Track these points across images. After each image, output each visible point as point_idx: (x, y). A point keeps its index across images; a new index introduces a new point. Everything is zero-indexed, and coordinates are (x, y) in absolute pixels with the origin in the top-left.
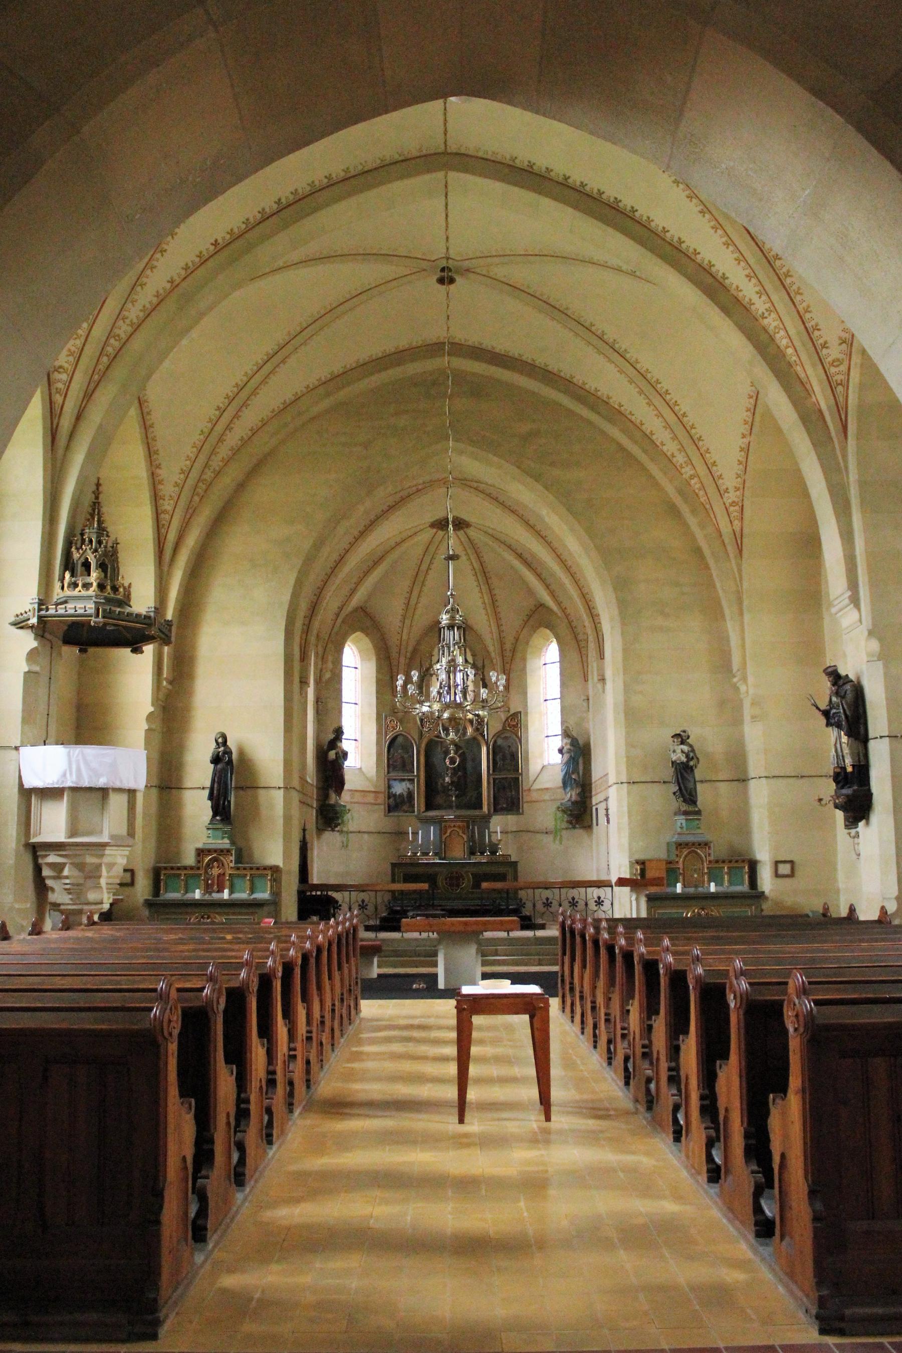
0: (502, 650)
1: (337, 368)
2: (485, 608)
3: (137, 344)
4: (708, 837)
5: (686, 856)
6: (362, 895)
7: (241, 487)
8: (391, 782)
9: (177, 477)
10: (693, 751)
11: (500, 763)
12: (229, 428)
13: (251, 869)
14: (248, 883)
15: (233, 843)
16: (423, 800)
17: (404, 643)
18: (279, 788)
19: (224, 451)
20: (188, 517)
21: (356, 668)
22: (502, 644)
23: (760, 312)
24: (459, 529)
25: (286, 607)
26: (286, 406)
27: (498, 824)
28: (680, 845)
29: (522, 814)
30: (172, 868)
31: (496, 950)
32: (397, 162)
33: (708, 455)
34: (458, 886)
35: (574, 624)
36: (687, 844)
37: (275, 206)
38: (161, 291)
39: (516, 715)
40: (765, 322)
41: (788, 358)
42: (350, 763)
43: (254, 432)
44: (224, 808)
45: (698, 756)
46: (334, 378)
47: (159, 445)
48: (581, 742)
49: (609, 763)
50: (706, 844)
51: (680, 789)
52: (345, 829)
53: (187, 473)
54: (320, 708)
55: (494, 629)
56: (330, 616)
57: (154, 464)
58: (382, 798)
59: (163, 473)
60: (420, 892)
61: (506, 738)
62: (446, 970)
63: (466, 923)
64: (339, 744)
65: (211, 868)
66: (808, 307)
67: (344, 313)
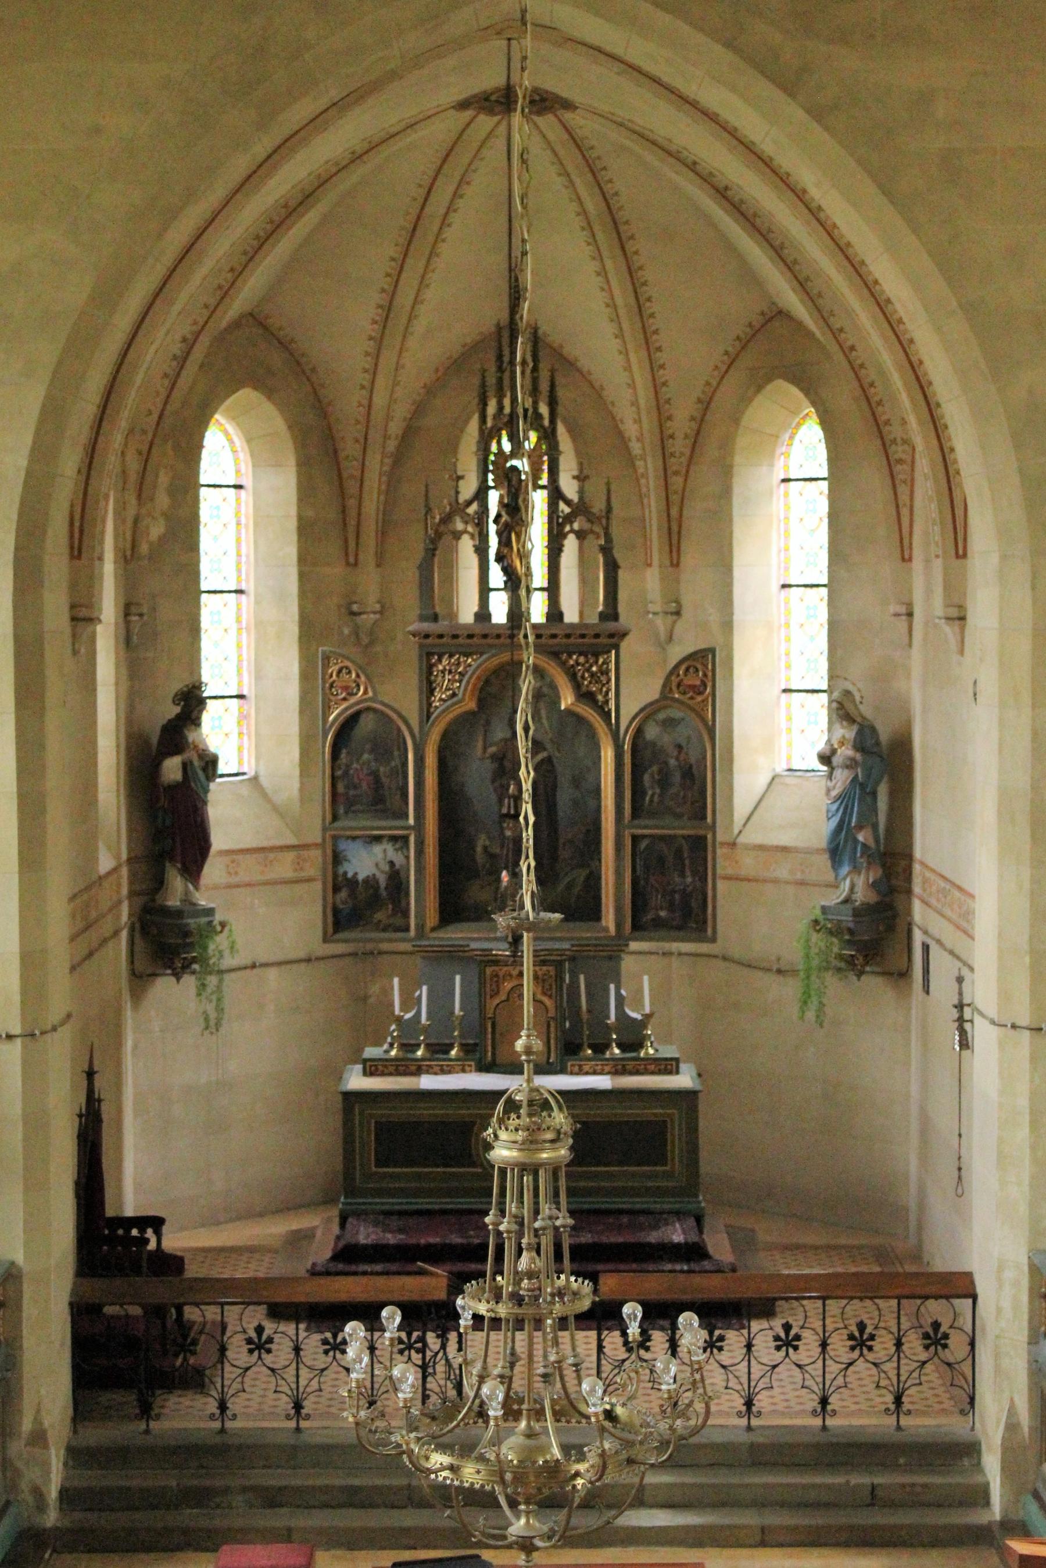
0: (664, 438)
2: (616, 319)
8: (342, 845)
11: (652, 792)
17: (378, 416)
18: (10, 1037)
21: (239, 496)
24: (539, 113)
27: (646, 982)
61: (670, 723)
64: (191, 736)
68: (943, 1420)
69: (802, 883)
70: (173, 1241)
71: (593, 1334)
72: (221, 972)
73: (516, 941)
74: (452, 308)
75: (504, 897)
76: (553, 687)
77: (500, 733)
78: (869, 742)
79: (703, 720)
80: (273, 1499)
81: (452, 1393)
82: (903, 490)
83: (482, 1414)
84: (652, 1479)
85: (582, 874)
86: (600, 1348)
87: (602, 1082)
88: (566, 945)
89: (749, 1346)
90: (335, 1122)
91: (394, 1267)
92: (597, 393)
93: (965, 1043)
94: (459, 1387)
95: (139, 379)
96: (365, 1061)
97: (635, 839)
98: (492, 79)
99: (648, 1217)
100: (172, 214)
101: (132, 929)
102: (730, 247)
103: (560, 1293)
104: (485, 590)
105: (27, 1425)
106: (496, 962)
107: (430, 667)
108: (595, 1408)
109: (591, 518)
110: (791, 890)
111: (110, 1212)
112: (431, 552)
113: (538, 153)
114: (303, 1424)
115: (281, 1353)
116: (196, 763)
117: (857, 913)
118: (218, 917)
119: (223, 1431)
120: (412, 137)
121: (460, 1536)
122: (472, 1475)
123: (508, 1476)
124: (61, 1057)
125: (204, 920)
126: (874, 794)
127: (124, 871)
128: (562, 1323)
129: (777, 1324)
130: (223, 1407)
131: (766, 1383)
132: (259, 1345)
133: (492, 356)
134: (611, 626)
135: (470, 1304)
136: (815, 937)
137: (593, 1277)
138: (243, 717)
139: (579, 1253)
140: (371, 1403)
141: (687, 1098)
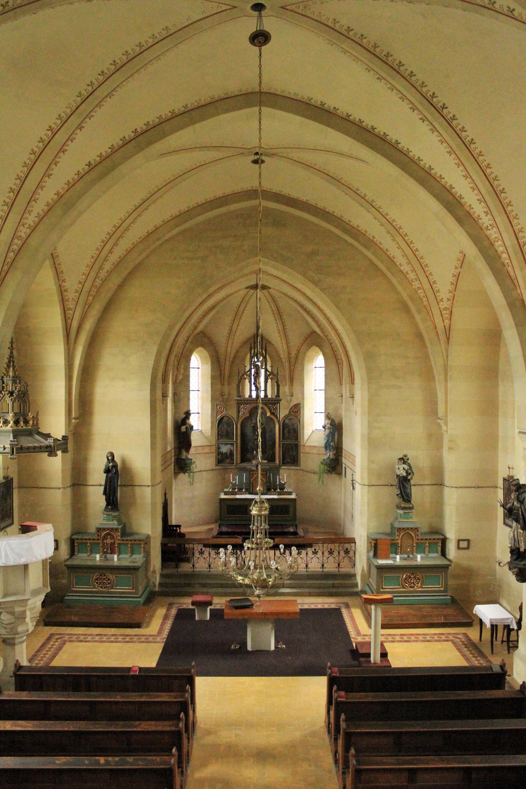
0: (289, 358)
1: (184, 207)
2: (279, 333)
3: (33, 242)
7: (121, 287)
8: (220, 445)
11: (287, 434)
12: (111, 252)
16: (239, 456)
17: (228, 354)
18: (148, 486)
19: (108, 266)
21: (199, 370)
22: (289, 354)
23: (485, 225)
26: (149, 234)
27: (285, 475)
28: (400, 529)
32: (223, 99)
33: (431, 277)
36: (404, 529)
37: (133, 135)
43: (129, 252)
44: (113, 502)
48: (337, 422)
49: (355, 446)
50: (416, 529)
51: (401, 493)
55: (285, 346)
57: (61, 279)
61: (290, 419)
64: (188, 421)
68: (348, 569)
69: (319, 454)
70: (183, 530)
71: (273, 551)
72: (194, 472)
73: (257, 466)
74: (244, 330)
75: (255, 456)
76: (266, 412)
77: (254, 421)
78: (333, 424)
79: (298, 419)
80: (204, 585)
81: (243, 563)
83: (249, 568)
84: (286, 582)
86: (275, 554)
87: (276, 497)
88: (268, 467)
89: (307, 554)
90: (218, 505)
91: (230, 536)
92: (277, 351)
93: (354, 488)
94: (244, 562)
95: (178, 345)
96: (224, 492)
98: (253, 282)
99: (286, 525)
100: (185, 311)
101: (175, 463)
102: (304, 319)
103: (266, 542)
104: (251, 390)
105: (152, 569)
106: (253, 471)
107: (239, 407)
108: (273, 567)
109: (274, 375)
111: (169, 524)
112: (239, 382)
113: (263, 299)
114: (211, 570)
115: (206, 554)
116: (189, 427)
118: (193, 461)
119: (193, 571)
120: (236, 295)
121: (244, 594)
122: (247, 581)
123: (255, 582)
124: (159, 490)
125: (190, 461)
126: (334, 435)
127: (173, 451)
128: (267, 549)
129: (313, 549)
130: (193, 566)
131: (311, 561)
132: (201, 553)
133: (253, 340)
134: (278, 398)
135: (246, 545)
136: (322, 465)
137: (273, 539)
138: (199, 417)
139: (270, 534)
140: (225, 566)
141: (294, 500)
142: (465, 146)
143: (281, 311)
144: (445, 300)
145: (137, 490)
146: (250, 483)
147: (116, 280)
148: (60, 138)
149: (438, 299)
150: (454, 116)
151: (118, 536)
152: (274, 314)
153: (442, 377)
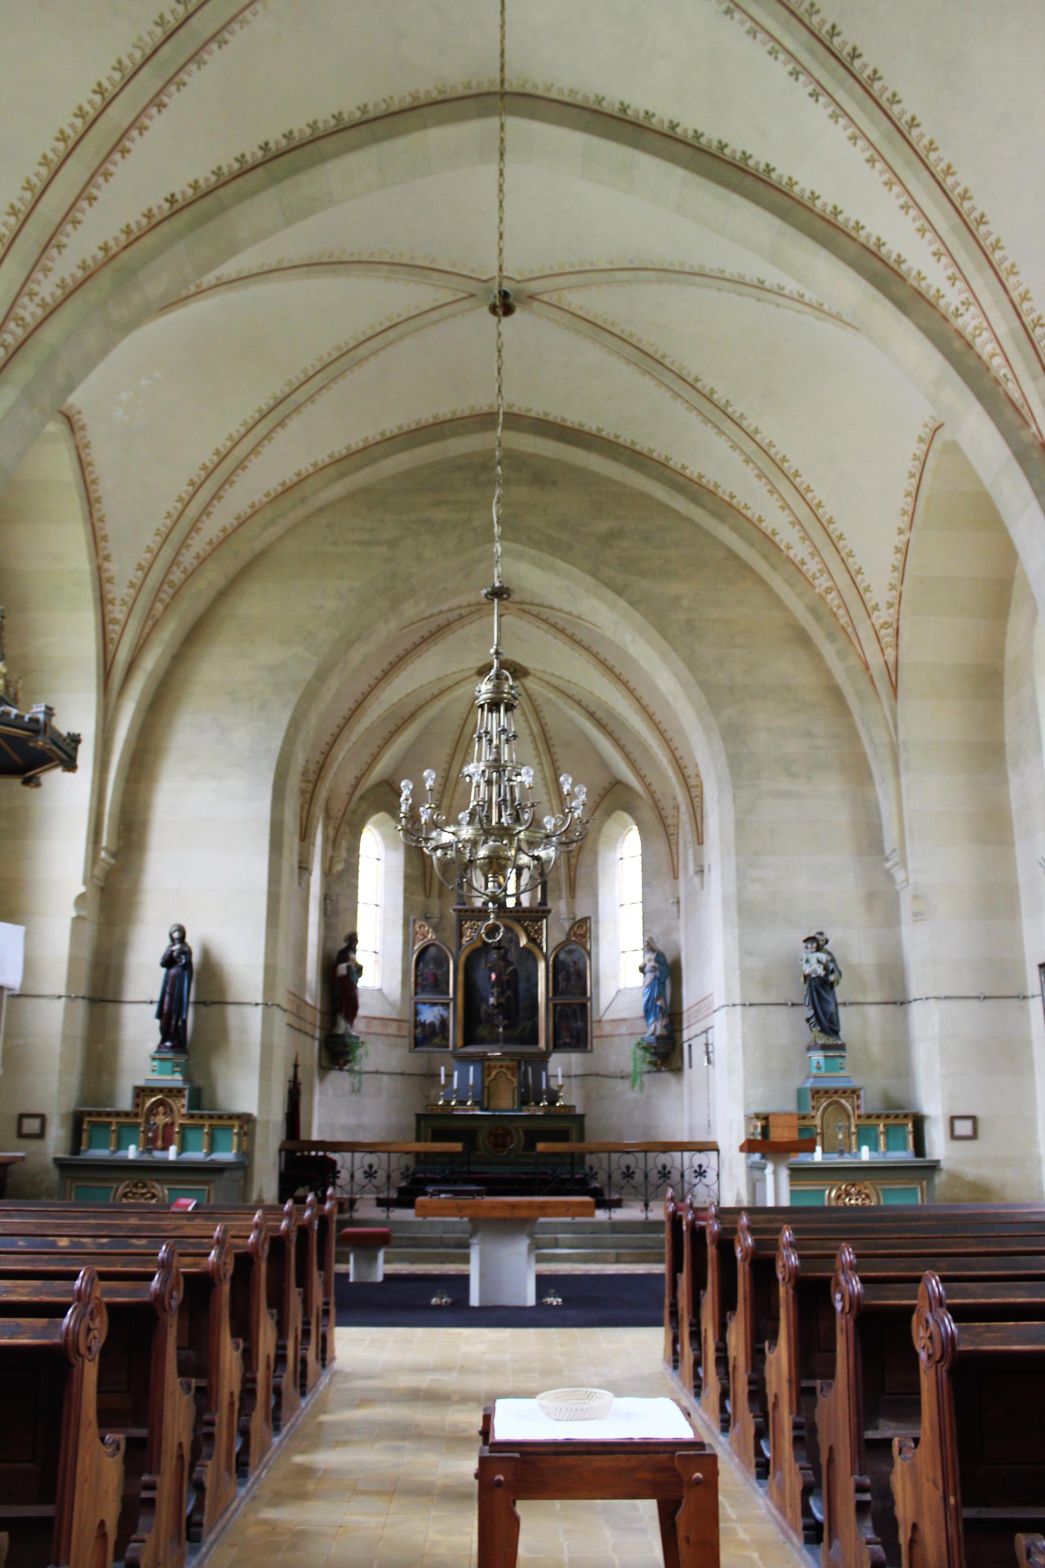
1: (356, 441)
3: (50, 334)
4: (855, 1082)
5: (826, 1108)
6: (370, 1158)
7: (223, 595)
8: (420, 1007)
9: (134, 575)
10: (833, 960)
11: (562, 984)
12: (206, 512)
13: (211, 1117)
14: (206, 1137)
15: (187, 1079)
18: (257, 1004)
19: (199, 544)
20: (146, 630)
21: (378, 862)
23: (952, 309)
25: (276, 756)
26: (287, 489)
28: (817, 1092)
29: (591, 1051)
30: (99, 1114)
31: (556, 1239)
34: (505, 1146)
35: (661, 804)
36: (827, 1092)
38: (90, 262)
39: (585, 920)
40: (959, 323)
41: (993, 372)
42: (363, 983)
43: (242, 522)
45: (841, 968)
46: (350, 455)
47: (109, 528)
48: (669, 958)
49: (714, 984)
50: (854, 1092)
51: (816, 1014)
52: (357, 1068)
53: (146, 570)
54: (329, 907)
56: (344, 789)
57: (101, 553)
58: (407, 1029)
59: (113, 568)
60: (451, 1154)
61: (571, 952)
62: (482, 1276)
63: (513, 1206)
64: (352, 956)
65: (155, 1115)
66: (1027, 292)
67: (366, 358)
79: (585, 949)
82: (674, 847)
85: (530, 1023)
97: (555, 1005)
110: (627, 1038)
116: (354, 968)
117: (658, 1038)
126: (664, 983)
134: (544, 908)
138: (377, 962)
142: (900, 139)
143: (548, 735)
144: (883, 606)
145: (232, 1013)
146: (483, 1088)
147: (213, 577)
148: (119, 114)
149: (869, 605)
150: (875, 72)
151: (183, 1106)
152: (535, 741)
153: (888, 767)
